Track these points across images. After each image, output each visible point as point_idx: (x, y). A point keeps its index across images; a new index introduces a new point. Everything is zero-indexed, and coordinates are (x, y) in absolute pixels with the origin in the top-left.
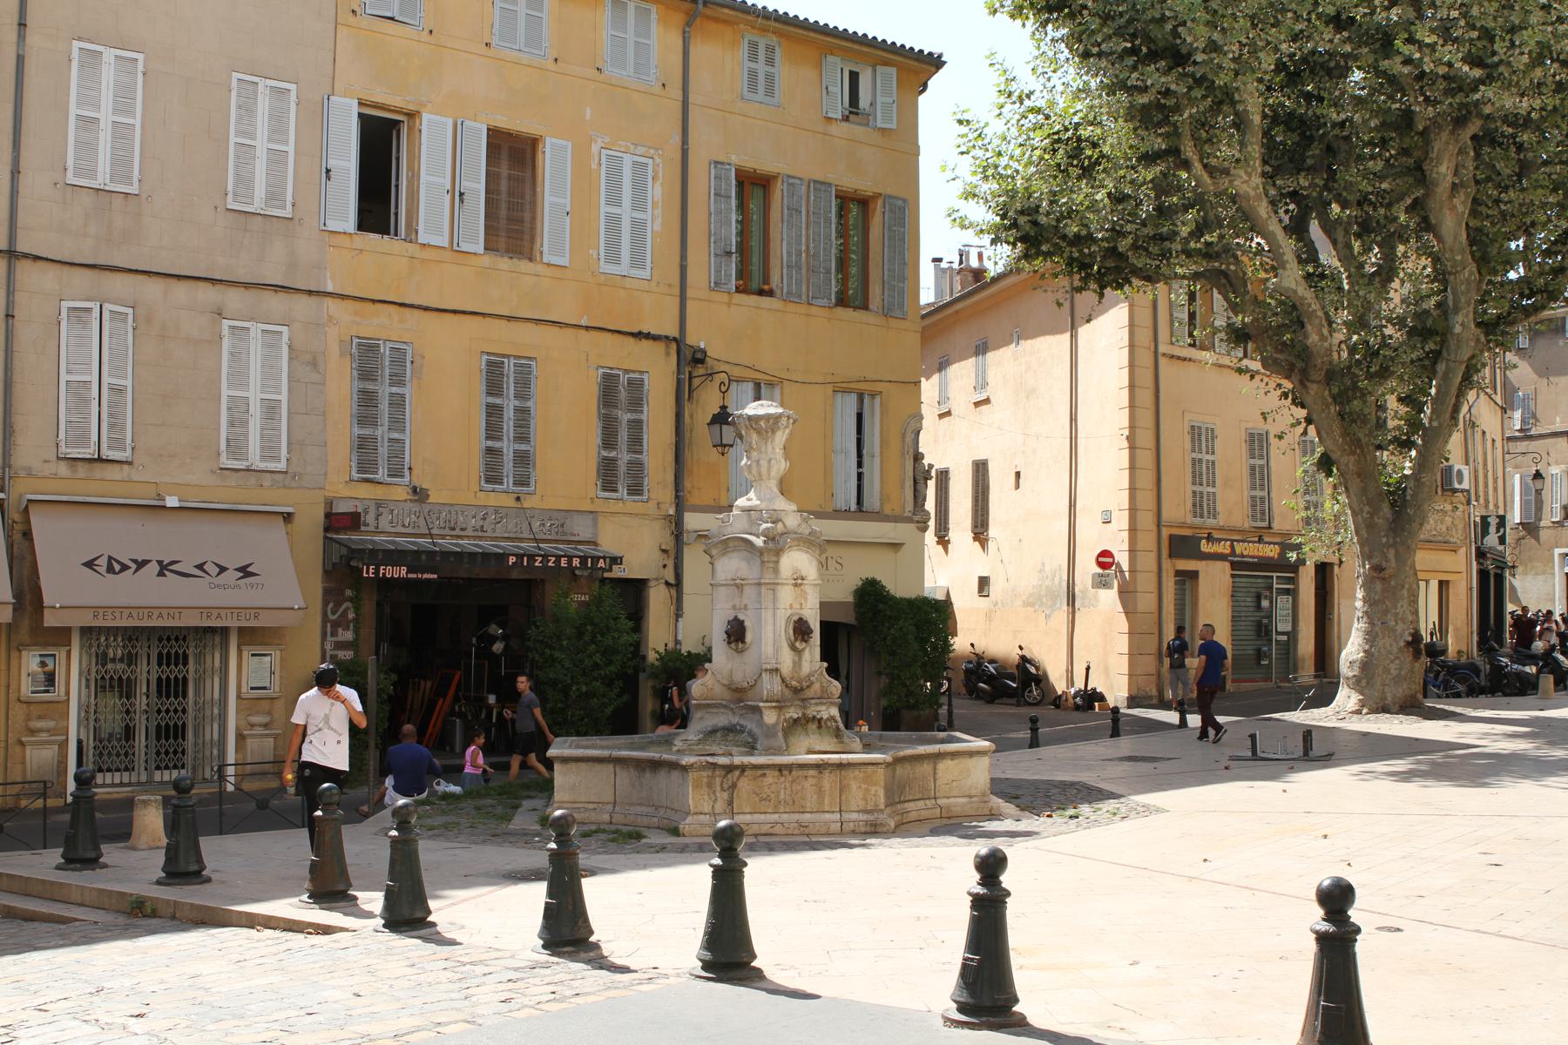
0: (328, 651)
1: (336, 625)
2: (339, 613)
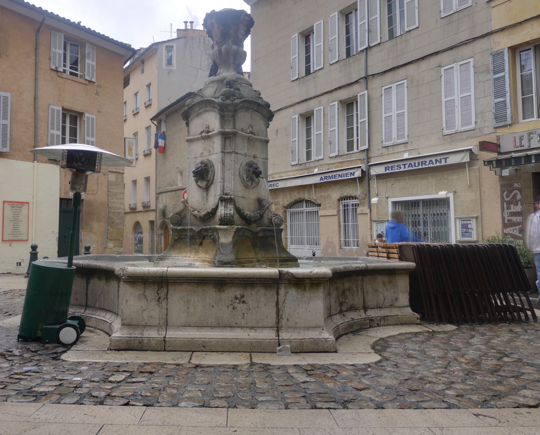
0: (506, 217)
1: (509, 203)
2: (511, 197)
